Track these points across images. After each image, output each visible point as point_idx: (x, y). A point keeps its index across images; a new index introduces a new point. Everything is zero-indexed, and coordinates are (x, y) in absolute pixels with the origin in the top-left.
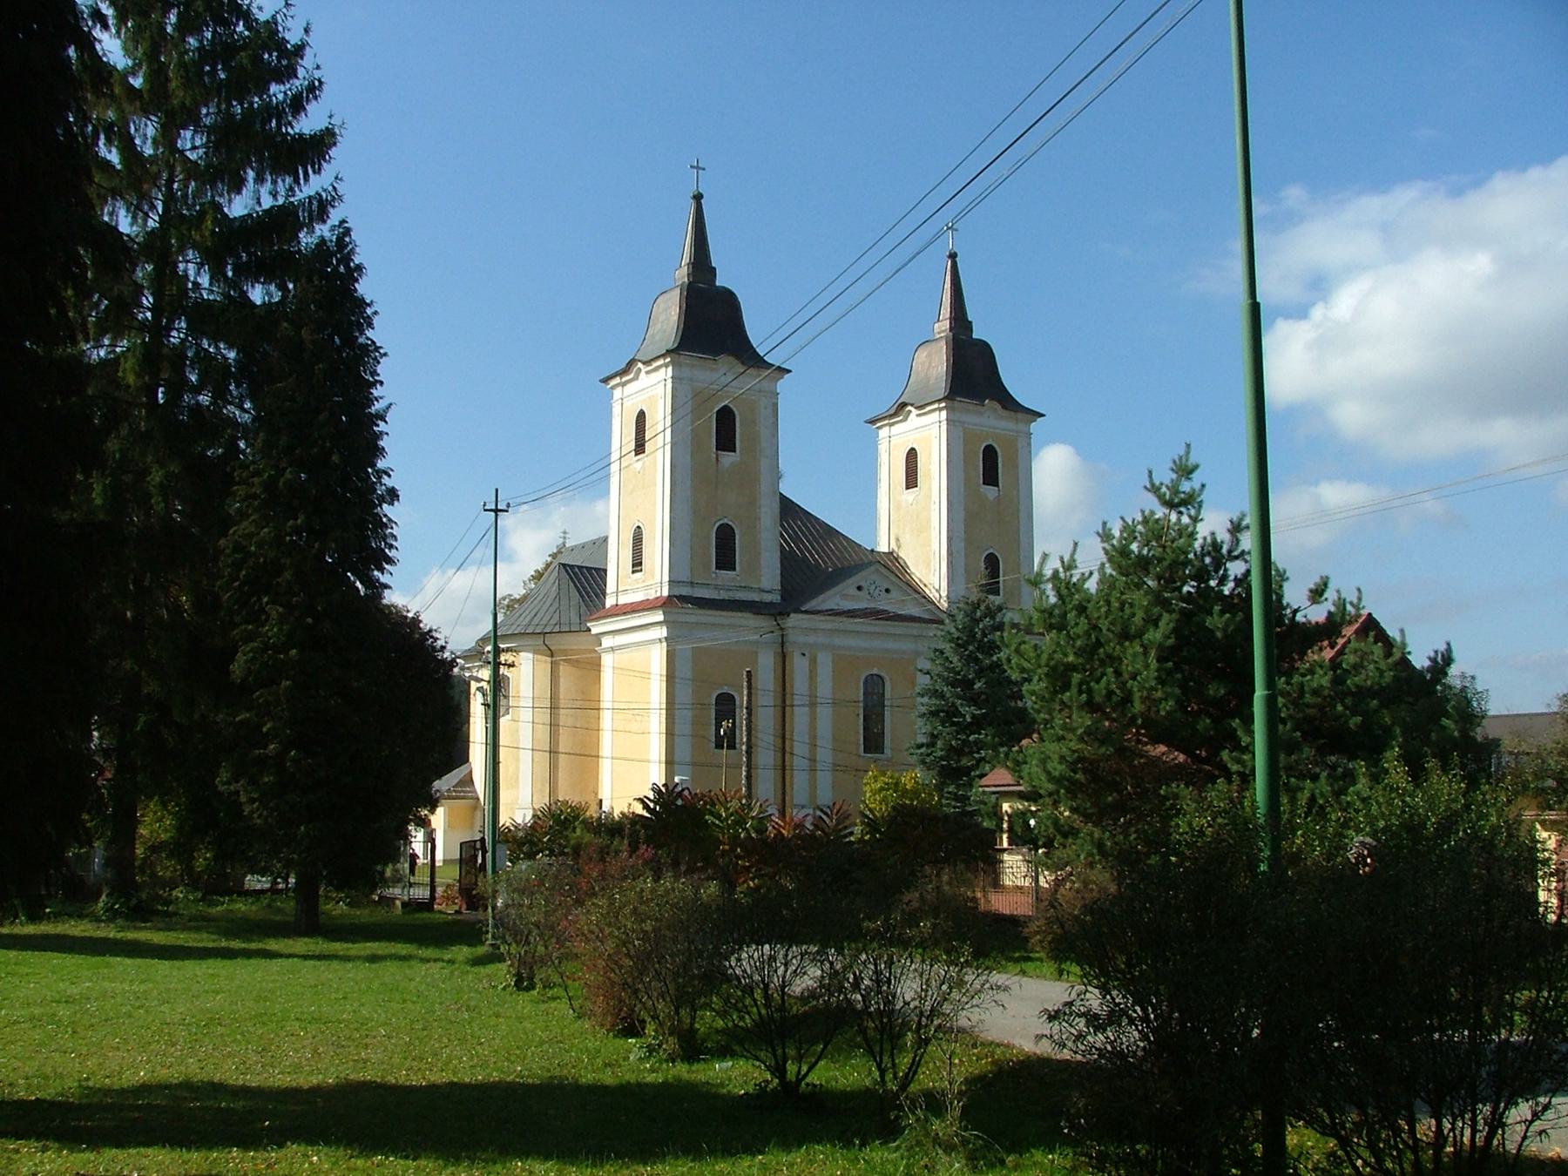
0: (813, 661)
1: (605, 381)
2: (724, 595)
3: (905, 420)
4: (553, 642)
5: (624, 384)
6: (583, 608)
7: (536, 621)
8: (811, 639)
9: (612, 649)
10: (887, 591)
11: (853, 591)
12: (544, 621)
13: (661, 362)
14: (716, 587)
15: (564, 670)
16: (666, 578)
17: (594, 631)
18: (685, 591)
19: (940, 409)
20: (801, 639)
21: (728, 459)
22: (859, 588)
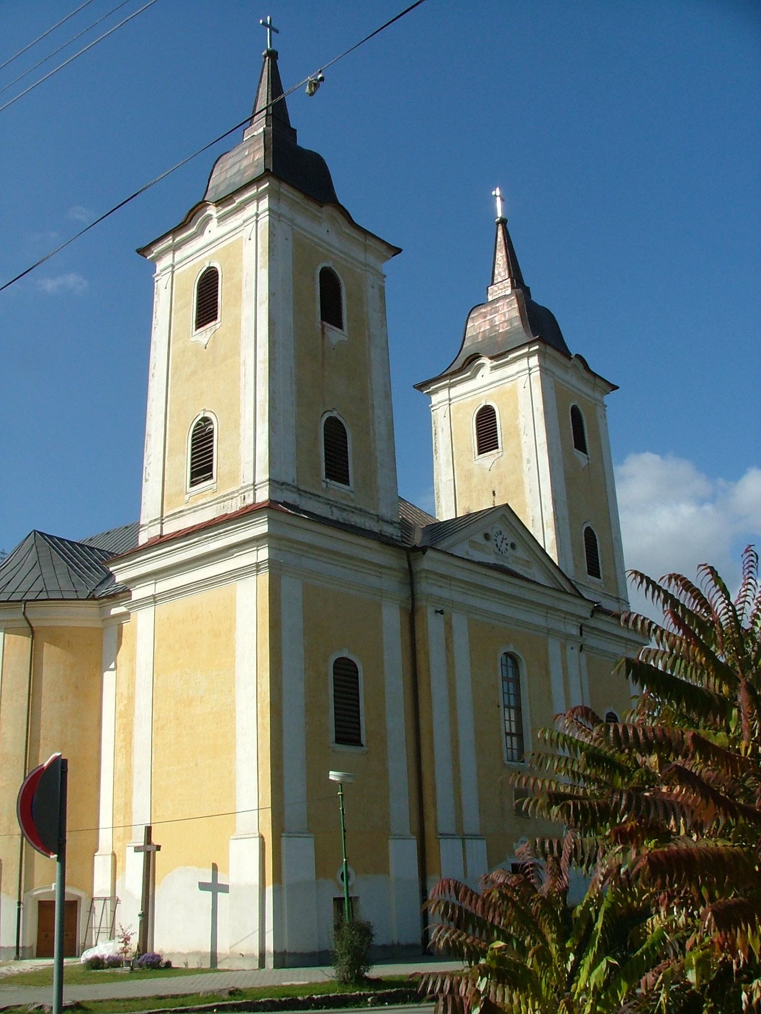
0: (448, 625)
1: (143, 251)
2: (336, 515)
3: (473, 377)
4: (41, 616)
5: (175, 248)
6: (75, 578)
7: (11, 588)
8: (445, 593)
9: (154, 599)
10: (513, 546)
11: (479, 538)
12: (24, 587)
13: (253, 191)
14: (329, 503)
15: (49, 652)
16: (263, 475)
17: (119, 578)
18: (291, 497)
19: (529, 355)
20: (435, 591)
21: (335, 335)
22: (487, 537)
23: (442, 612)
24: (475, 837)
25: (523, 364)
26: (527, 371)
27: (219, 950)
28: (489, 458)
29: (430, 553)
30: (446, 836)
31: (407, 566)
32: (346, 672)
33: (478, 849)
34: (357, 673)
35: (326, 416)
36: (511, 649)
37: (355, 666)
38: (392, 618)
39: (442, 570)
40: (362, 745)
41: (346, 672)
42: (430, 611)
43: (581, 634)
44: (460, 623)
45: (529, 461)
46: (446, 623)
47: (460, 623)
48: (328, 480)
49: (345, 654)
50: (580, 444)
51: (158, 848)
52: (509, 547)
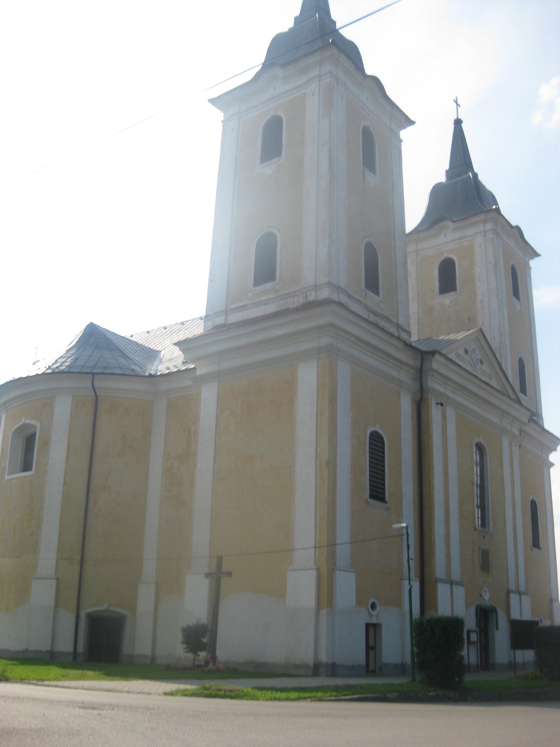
2: (372, 318)
10: (481, 362)
11: (462, 353)
14: (366, 307)
22: (466, 351)
23: (442, 404)
24: (460, 584)
25: (481, 228)
26: (483, 233)
27: (306, 655)
28: (447, 299)
29: (437, 357)
30: (442, 581)
31: (419, 365)
32: (376, 443)
33: (460, 592)
34: (383, 444)
35: (366, 240)
36: (481, 440)
37: (382, 439)
38: (406, 405)
39: (443, 371)
40: (386, 502)
41: (376, 443)
42: (433, 402)
43: (520, 434)
44: (451, 413)
45: (482, 302)
46: (442, 414)
47: (451, 413)
48: (366, 290)
49: (378, 428)
50: (516, 294)
51: (230, 574)
52: (479, 362)
